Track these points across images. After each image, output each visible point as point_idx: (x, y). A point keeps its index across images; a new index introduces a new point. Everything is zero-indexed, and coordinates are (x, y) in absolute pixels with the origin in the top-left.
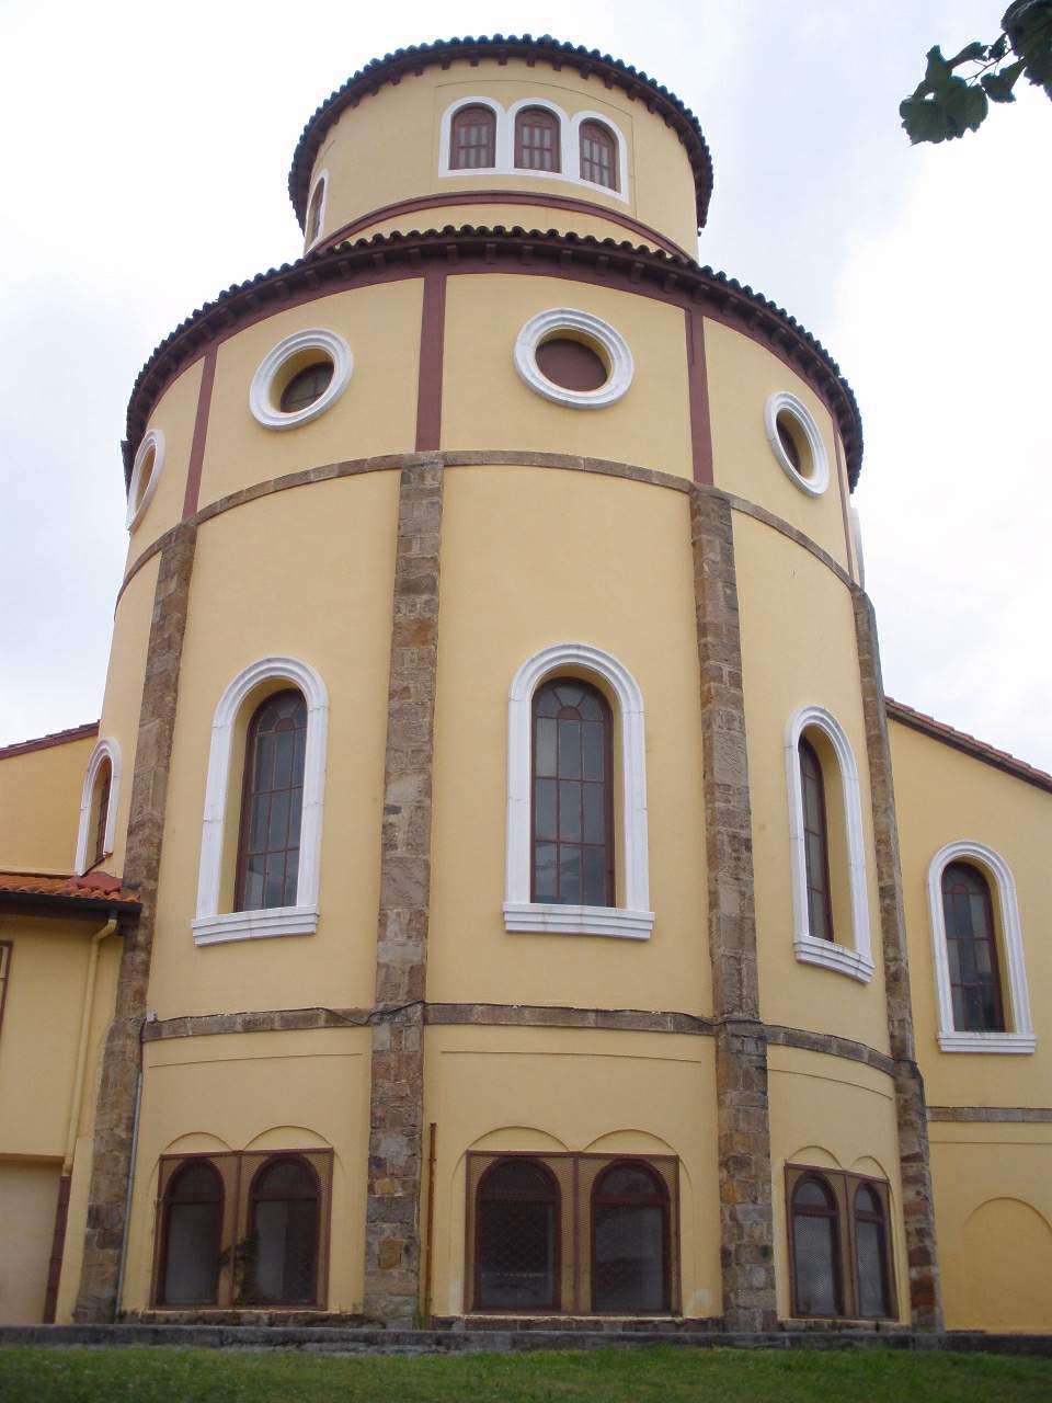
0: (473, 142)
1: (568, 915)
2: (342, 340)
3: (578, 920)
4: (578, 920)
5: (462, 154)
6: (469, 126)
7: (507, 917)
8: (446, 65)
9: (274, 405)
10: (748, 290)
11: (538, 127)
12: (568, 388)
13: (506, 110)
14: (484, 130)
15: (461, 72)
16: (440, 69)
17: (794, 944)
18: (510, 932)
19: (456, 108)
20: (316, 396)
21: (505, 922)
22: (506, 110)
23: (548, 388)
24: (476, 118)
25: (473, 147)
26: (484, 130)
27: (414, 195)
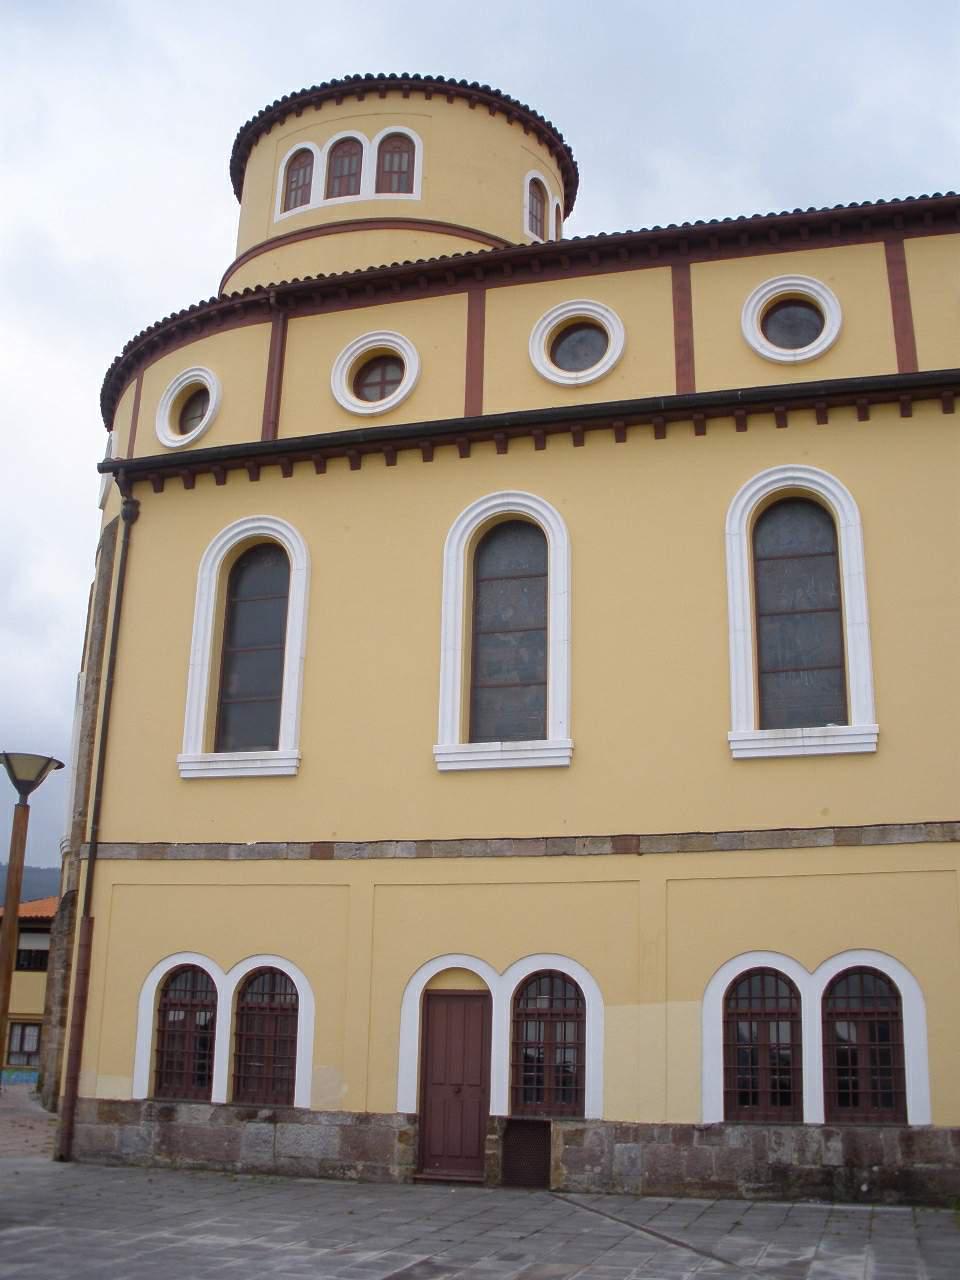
0: (396, 169)
1: (492, 752)
2: (210, 371)
3: (822, 742)
4: (822, 742)
5: (337, 184)
6: (392, 153)
7: (438, 759)
8: (318, 106)
9: (175, 432)
10: (192, 308)
11: (396, 152)
12: (592, 365)
13: (371, 141)
14: (355, 159)
15: (394, 102)
16: (356, 99)
17: (729, 742)
18: (184, 779)
19: (331, 144)
20: (202, 416)
21: (731, 750)
22: (371, 141)
23: (772, 352)
24: (346, 150)
25: (396, 172)
26: (405, 156)
27: (453, 221)
